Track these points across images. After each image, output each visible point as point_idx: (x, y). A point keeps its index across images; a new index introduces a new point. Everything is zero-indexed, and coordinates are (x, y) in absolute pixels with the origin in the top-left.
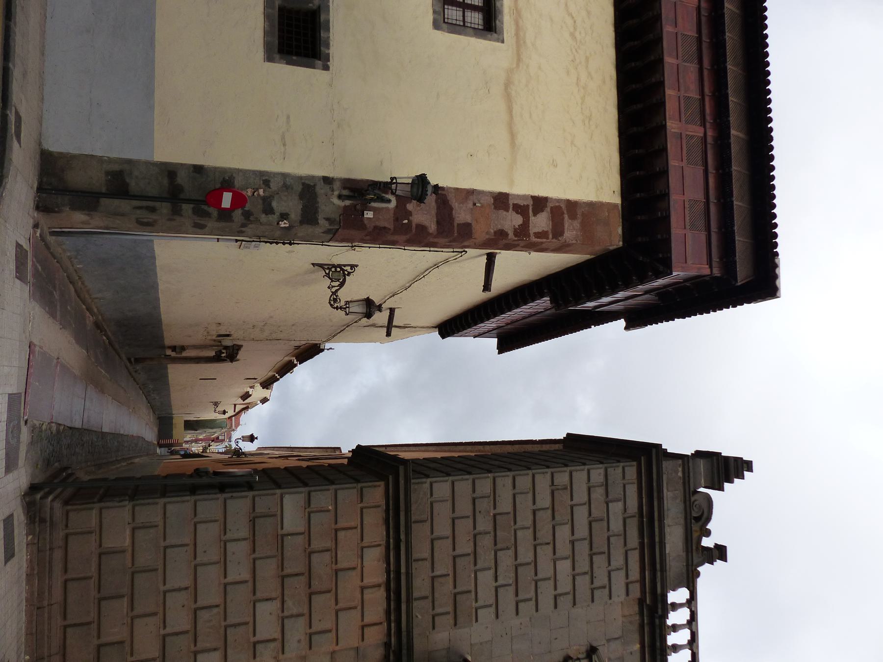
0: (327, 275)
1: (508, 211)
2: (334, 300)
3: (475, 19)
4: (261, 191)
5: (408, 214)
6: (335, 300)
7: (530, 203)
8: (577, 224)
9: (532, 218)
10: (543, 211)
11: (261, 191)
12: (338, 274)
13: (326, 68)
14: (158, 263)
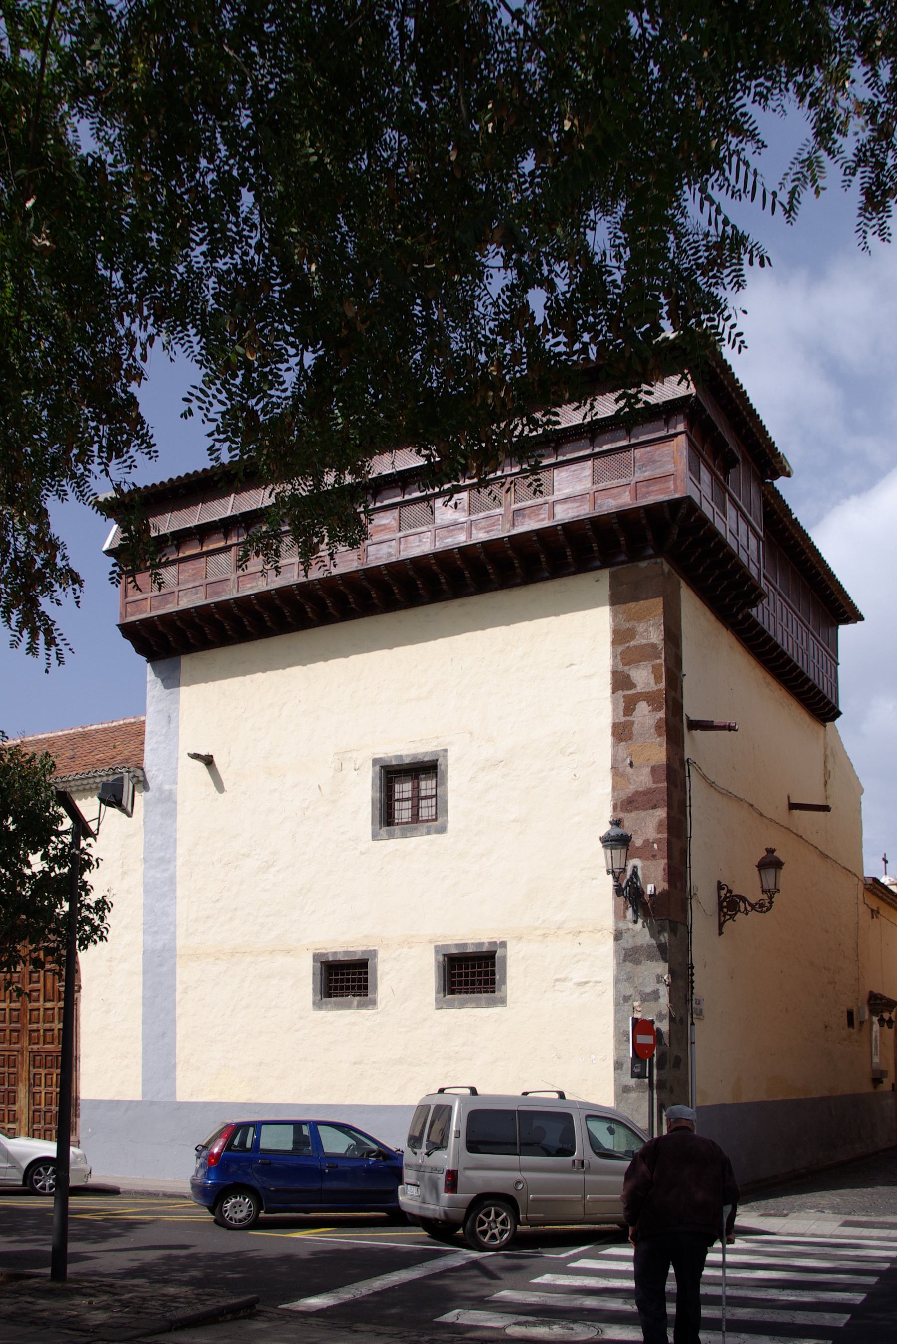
0: (732, 917)
1: (633, 722)
2: (761, 907)
3: (426, 786)
4: (636, 1004)
5: (647, 843)
6: (762, 906)
7: (620, 693)
8: (641, 628)
9: (639, 689)
10: (629, 676)
11: (636, 1004)
12: (729, 904)
13: (503, 944)
14: (728, 1099)
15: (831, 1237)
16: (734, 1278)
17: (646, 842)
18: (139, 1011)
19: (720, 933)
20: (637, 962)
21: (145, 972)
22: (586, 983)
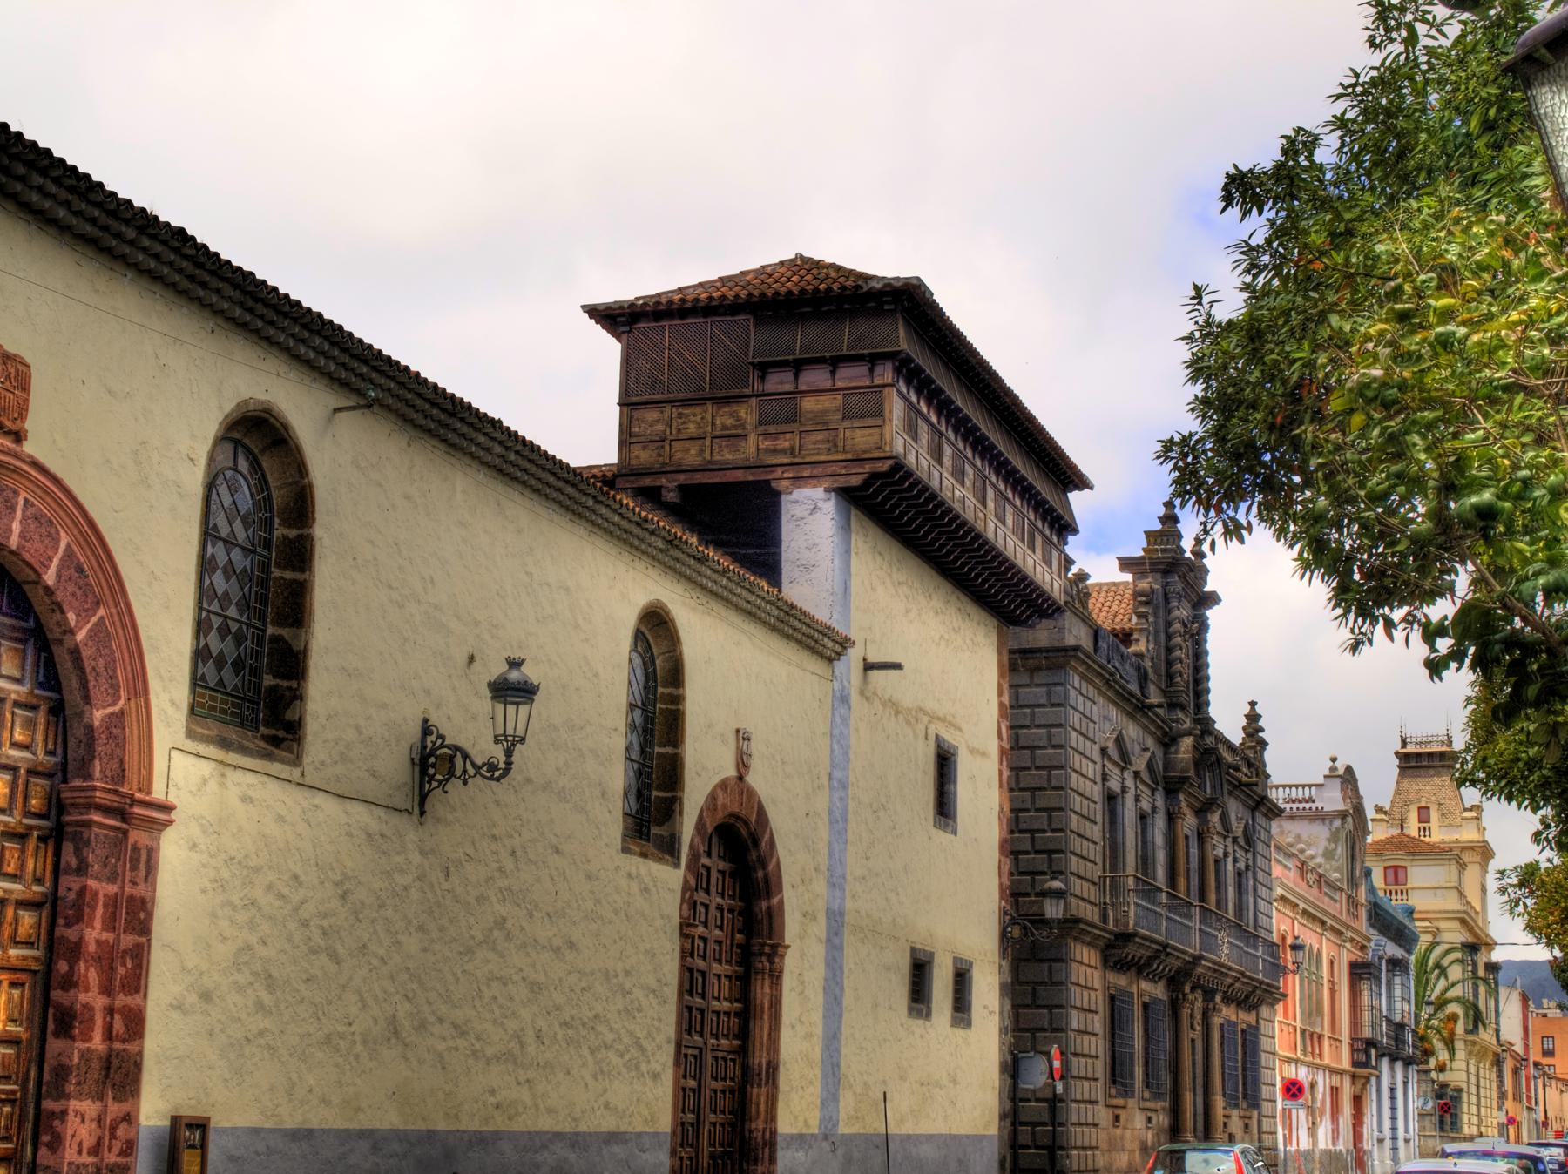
6: (493, 767)
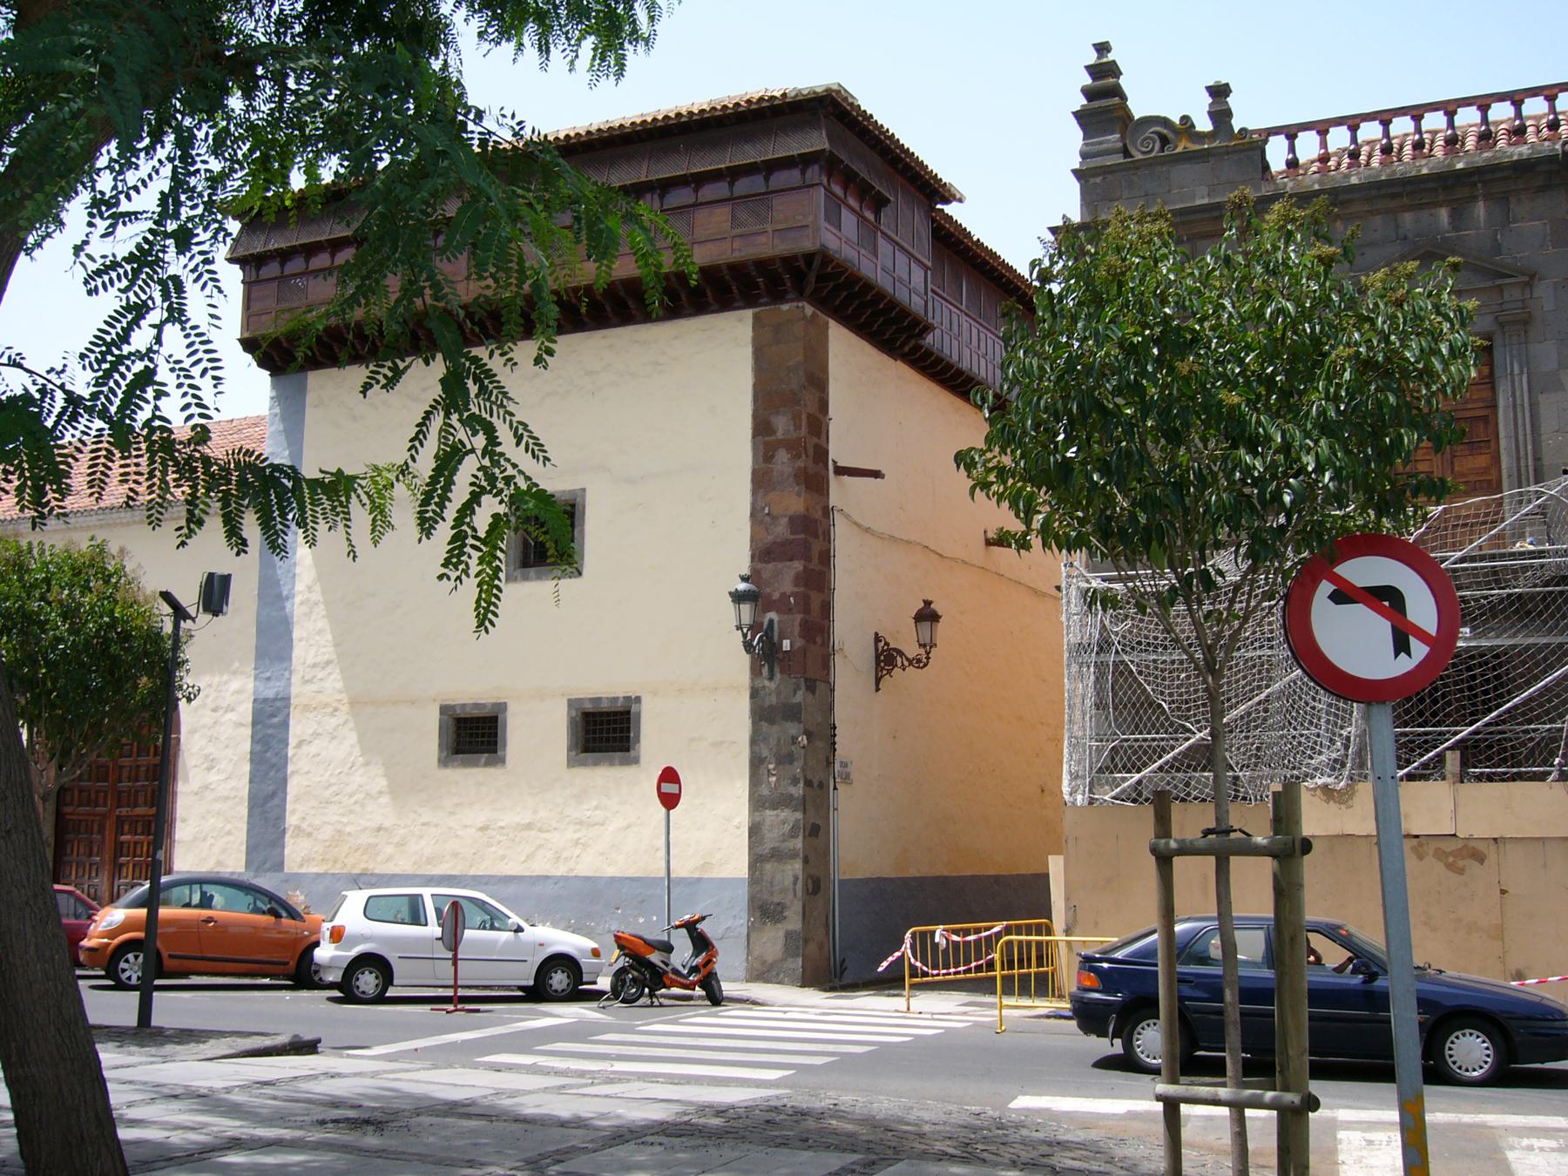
0: (889, 672)
2: (919, 663)
5: (784, 596)
6: (919, 661)
9: (780, 435)
13: (638, 700)
14: (888, 873)
15: (478, 1011)
16: (1457, 1110)
17: (783, 595)
18: (247, 768)
19: (878, 689)
20: (772, 722)
21: (254, 724)
22: (722, 742)
